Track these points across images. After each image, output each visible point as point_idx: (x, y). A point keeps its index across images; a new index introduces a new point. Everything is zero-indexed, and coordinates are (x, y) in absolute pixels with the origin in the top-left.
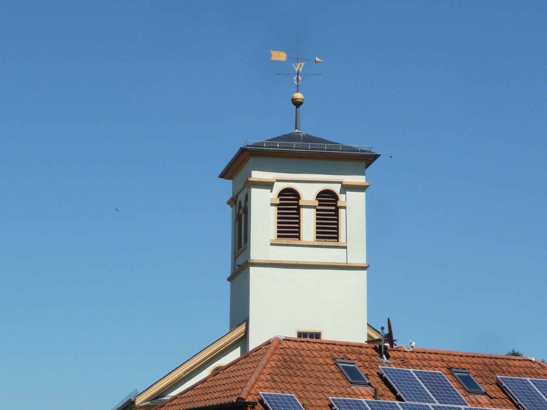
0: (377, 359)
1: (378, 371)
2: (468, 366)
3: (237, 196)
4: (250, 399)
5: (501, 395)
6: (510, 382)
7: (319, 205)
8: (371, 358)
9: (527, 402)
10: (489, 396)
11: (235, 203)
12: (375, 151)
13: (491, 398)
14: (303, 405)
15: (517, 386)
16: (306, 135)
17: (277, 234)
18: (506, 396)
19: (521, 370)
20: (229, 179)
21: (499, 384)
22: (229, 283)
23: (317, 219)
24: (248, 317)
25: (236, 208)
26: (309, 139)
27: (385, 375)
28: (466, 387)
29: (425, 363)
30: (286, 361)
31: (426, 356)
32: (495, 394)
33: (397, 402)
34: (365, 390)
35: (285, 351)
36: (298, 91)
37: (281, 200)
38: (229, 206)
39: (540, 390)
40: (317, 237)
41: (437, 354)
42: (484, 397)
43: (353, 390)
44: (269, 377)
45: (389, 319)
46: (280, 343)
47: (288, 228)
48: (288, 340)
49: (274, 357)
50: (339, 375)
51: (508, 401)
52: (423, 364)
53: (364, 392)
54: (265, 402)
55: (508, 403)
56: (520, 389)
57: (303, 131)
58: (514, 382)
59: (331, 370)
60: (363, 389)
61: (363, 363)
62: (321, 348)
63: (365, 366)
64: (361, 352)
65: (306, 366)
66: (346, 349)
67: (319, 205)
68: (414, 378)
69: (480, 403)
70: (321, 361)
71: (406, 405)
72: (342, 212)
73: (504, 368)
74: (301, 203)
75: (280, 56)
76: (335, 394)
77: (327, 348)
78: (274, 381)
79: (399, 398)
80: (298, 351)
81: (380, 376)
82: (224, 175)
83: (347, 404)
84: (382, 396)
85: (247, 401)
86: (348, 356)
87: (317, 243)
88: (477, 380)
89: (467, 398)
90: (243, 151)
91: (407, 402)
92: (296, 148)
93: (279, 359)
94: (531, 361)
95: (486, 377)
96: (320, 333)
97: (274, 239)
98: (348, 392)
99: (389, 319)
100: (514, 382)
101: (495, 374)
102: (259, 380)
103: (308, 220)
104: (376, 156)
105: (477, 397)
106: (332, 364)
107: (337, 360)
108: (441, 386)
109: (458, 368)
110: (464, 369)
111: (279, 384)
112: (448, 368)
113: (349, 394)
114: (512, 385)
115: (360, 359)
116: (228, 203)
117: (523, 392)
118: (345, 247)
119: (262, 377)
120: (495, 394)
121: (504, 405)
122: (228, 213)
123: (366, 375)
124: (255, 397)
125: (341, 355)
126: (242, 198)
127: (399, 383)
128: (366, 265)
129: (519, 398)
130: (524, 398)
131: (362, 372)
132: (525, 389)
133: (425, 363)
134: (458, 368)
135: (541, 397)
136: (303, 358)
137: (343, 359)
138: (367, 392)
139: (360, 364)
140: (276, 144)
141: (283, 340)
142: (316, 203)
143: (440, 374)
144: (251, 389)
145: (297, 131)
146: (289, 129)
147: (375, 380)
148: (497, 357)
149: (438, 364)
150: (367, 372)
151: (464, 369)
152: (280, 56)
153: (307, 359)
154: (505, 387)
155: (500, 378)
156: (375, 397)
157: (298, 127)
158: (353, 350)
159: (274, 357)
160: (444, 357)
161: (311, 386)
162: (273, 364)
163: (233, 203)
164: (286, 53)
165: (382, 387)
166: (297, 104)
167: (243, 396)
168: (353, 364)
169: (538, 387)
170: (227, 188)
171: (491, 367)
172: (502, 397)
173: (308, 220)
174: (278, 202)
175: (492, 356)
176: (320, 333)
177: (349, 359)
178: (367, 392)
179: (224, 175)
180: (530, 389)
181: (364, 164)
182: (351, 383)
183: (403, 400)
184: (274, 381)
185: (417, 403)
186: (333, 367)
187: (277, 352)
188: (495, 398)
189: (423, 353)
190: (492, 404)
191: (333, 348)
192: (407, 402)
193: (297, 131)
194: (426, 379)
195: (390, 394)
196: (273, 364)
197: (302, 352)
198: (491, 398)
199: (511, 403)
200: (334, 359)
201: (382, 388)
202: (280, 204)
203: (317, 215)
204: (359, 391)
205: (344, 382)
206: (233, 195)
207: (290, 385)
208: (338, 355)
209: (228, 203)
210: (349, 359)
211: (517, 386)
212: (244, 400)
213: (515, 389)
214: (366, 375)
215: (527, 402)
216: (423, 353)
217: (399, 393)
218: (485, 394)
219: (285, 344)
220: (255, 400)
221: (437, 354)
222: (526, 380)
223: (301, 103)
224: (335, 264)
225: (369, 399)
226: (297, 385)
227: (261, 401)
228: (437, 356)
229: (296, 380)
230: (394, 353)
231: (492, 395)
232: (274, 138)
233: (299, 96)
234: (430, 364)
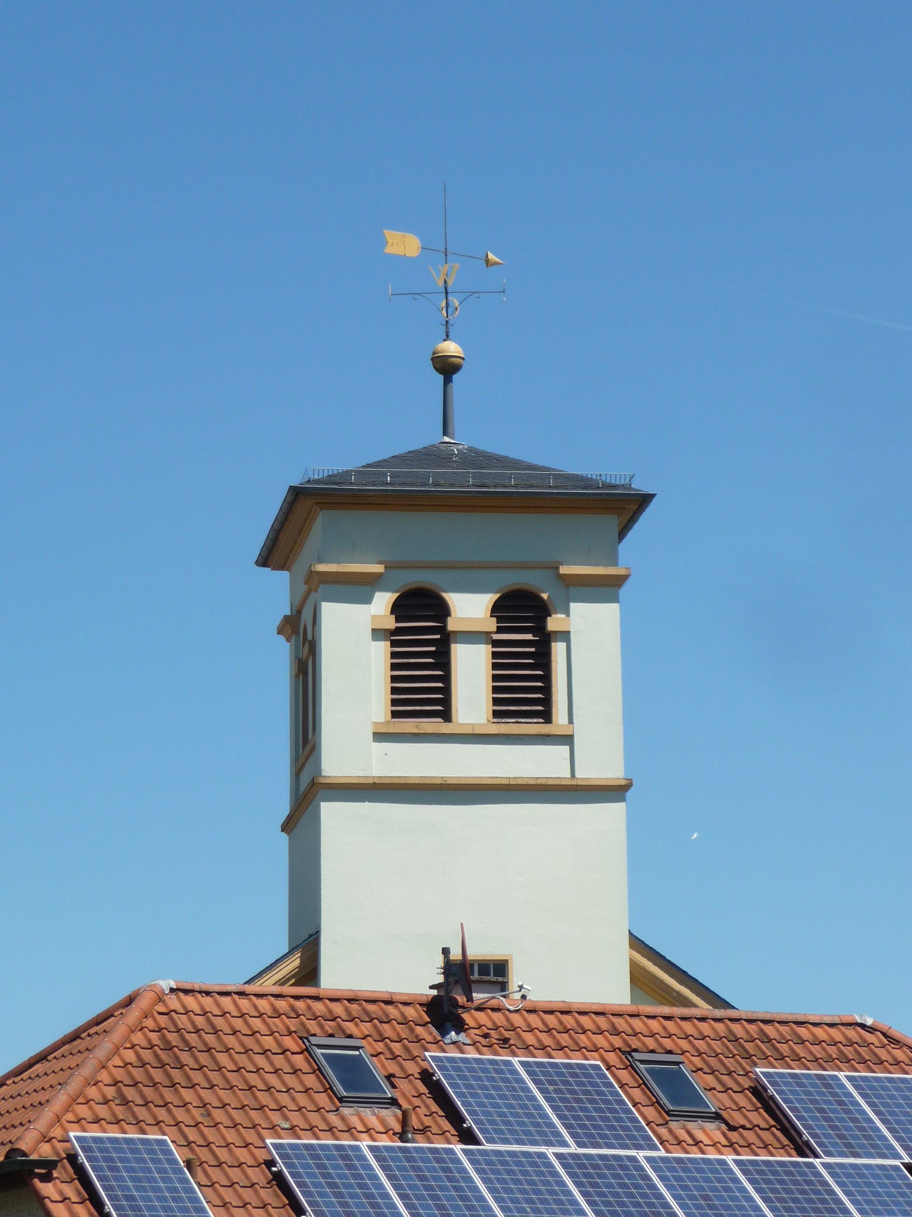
0: (427, 1033)
1: (424, 1065)
2: (684, 1045)
3: (299, 612)
4: (46, 1151)
5: (760, 1118)
6: (787, 1084)
7: (500, 630)
8: (412, 1030)
9: (827, 1136)
10: (727, 1123)
11: (295, 631)
12: (641, 485)
13: (732, 1128)
14: (189, 1164)
15: (808, 1093)
16: (471, 449)
17: (390, 708)
18: (773, 1123)
19: (832, 1051)
20: (282, 568)
21: (758, 1092)
22: (285, 837)
23: (495, 666)
24: (319, 926)
25: (297, 642)
26: (476, 459)
27: (439, 1075)
28: (665, 1101)
29: (564, 1039)
30: (169, 1048)
31: (568, 1020)
32: (746, 1117)
33: (458, 1148)
34: (378, 1118)
35: (172, 1019)
36: (447, 337)
37: (398, 620)
38: (282, 638)
39: (871, 1104)
40: (496, 714)
41: (602, 1014)
42: (710, 1126)
43: (343, 1119)
44: (110, 1092)
45: (462, 924)
46: (160, 999)
47: (420, 694)
48: (186, 992)
49: (138, 1038)
50: (311, 1081)
51: (778, 1133)
52: (558, 1043)
53: (373, 1122)
54: (82, 1158)
55: (778, 1139)
56: (814, 1102)
57: (464, 438)
58: (801, 1085)
59: (292, 1066)
60: (371, 1116)
61: (387, 1046)
62: (275, 1009)
63: (392, 1052)
64: (387, 1015)
65: (223, 1059)
66: (347, 1010)
67: (500, 630)
68: (521, 1081)
69: (697, 1143)
70: (268, 1042)
71: (484, 1153)
72: (558, 649)
73: (783, 1048)
74: (452, 625)
75: (404, 244)
76: (293, 1130)
77: (292, 1008)
78: (125, 1102)
79: (467, 1137)
80: (208, 1020)
81: (426, 1076)
82: (266, 559)
83: (316, 1157)
84: (424, 1130)
85: (32, 1157)
86: (350, 1027)
87: (495, 729)
88: (698, 1082)
89: (663, 1131)
90: (296, 494)
91: (488, 1147)
92: (434, 485)
93: (150, 1041)
94: (863, 1026)
95: (730, 1073)
96: (507, 961)
97: (381, 719)
98: (328, 1123)
99: (462, 924)
100: (801, 1085)
101: (755, 1064)
102: (81, 1100)
103: (472, 672)
104: (644, 500)
105: (691, 1126)
106: (297, 1050)
107: (314, 1040)
108: (592, 1101)
109: (653, 1051)
110: (670, 1052)
111: (136, 1109)
112: (623, 1052)
113: (331, 1129)
114: (793, 1092)
115: (380, 1034)
116: (280, 631)
117: (821, 1111)
118: (567, 739)
119: (92, 1092)
120: (746, 1117)
121: (749, 1146)
122: (281, 654)
123: (389, 1077)
124: (60, 1146)
125: (329, 1026)
126: (307, 616)
127: (474, 1095)
128: (623, 783)
129: (807, 1127)
130: (821, 1127)
131: (378, 1068)
132: (827, 1102)
133: (564, 1039)
134: (653, 1051)
135: (870, 1121)
136: (219, 1038)
137: (331, 1035)
138: (382, 1122)
139: (380, 1046)
140: (384, 475)
141: (172, 990)
142: (491, 625)
143: (597, 1067)
144: (52, 1126)
145: (447, 439)
146: (428, 434)
147: (409, 1091)
148: (768, 1017)
149: (600, 1040)
150: (392, 1067)
151: (670, 1052)
152: (404, 244)
153: (231, 1041)
154: (772, 1098)
155: (763, 1073)
156: (402, 1137)
157: (450, 430)
158: (365, 1011)
159: (138, 1038)
160: (620, 1023)
161: (227, 1113)
162: (130, 1055)
163: (288, 630)
164: (421, 241)
165: (428, 1107)
166: (447, 368)
167: (23, 1146)
168: (357, 1048)
169: (863, 1096)
170: (277, 590)
171: (748, 1046)
172: (763, 1125)
173: (472, 672)
174: (391, 623)
175: (754, 1017)
176: (507, 961)
177: (350, 1036)
178: (382, 1122)
179: (266, 559)
180: (844, 1102)
181: (612, 522)
182: (341, 1100)
183: (477, 1142)
184: (125, 1102)
185: (515, 1148)
186: (299, 1061)
187: (149, 1023)
188: (743, 1127)
189: (562, 1012)
190: (731, 1145)
191: (309, 1008)
192: (488, 1147)
193: (447, 439)
194: (551, 1083)
195: (447, 1126)
196: (130, 1055)
197: (219, 1022)
198: (732, 1128)
199: (785, 1141)
200: (305, 1037)
201: (425, 1111)
202: (397, 631)
203: (394, 655)
204: (362, 1120)
205: (323, 1099)
206: (292, 610)
207: (169, 1111)
208: (322, 1027)
209: (280, 631)
210: (350, 1036)
211: (808, 1093)
212: (24, 1154)
213: (800, 1101)
214: (389, 1077)
215: (827, 1136)
216: (562, 1012)
217: (470, 1122)
218: (717, 1117)
219: (173, 1002)
220: (57, 1154)
221: (602, 1014)
222: (835, 1078)
223: (456, 368)
224: (543, 782)
225: (384, 1142)
226: (188, 1111)
227: (72, 1158)
228: (601, 1020)
229: (188, 1095)
230: (481, 1017)
231: (737, 1119)
232: (385, 461)
233: (451, 348)
234: (576, 1043)
